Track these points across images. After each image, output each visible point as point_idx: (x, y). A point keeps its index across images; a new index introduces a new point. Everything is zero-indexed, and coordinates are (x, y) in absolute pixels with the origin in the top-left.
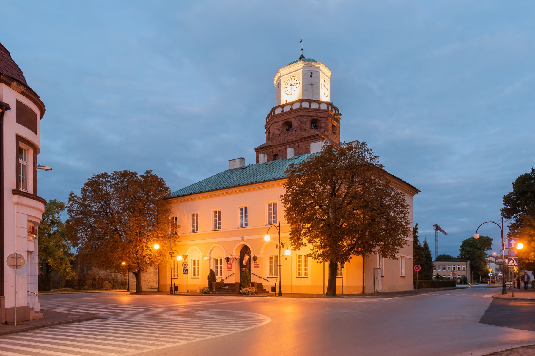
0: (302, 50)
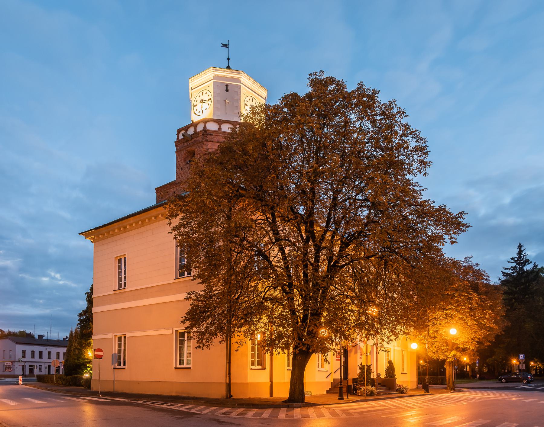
0: (228, 59)
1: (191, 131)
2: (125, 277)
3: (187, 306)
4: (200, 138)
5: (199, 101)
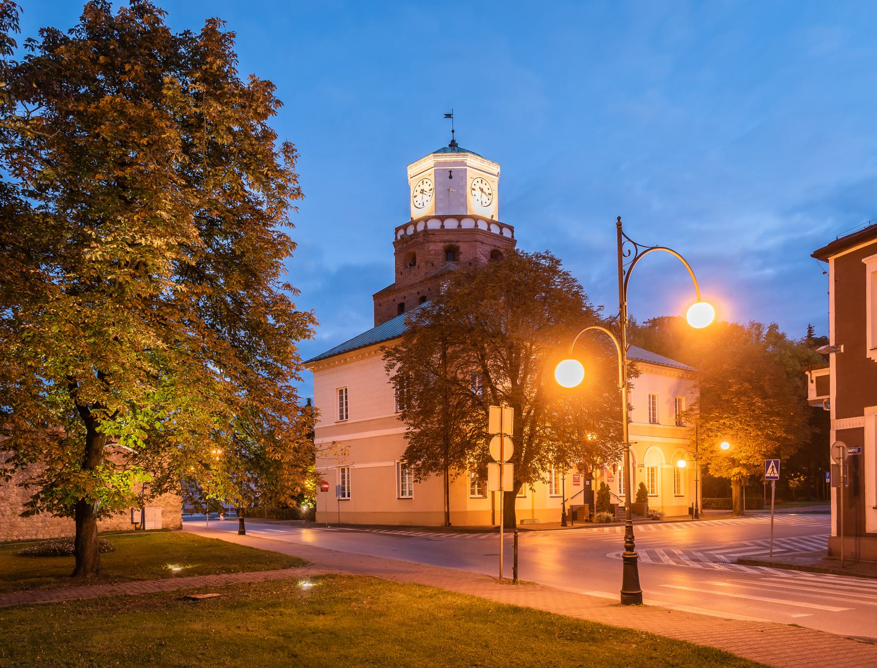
0: (453, 131)
1: (410, 231)
2: (347, 409)
3: (406, 444)
4: (421, 239)
5: (419, 191)
